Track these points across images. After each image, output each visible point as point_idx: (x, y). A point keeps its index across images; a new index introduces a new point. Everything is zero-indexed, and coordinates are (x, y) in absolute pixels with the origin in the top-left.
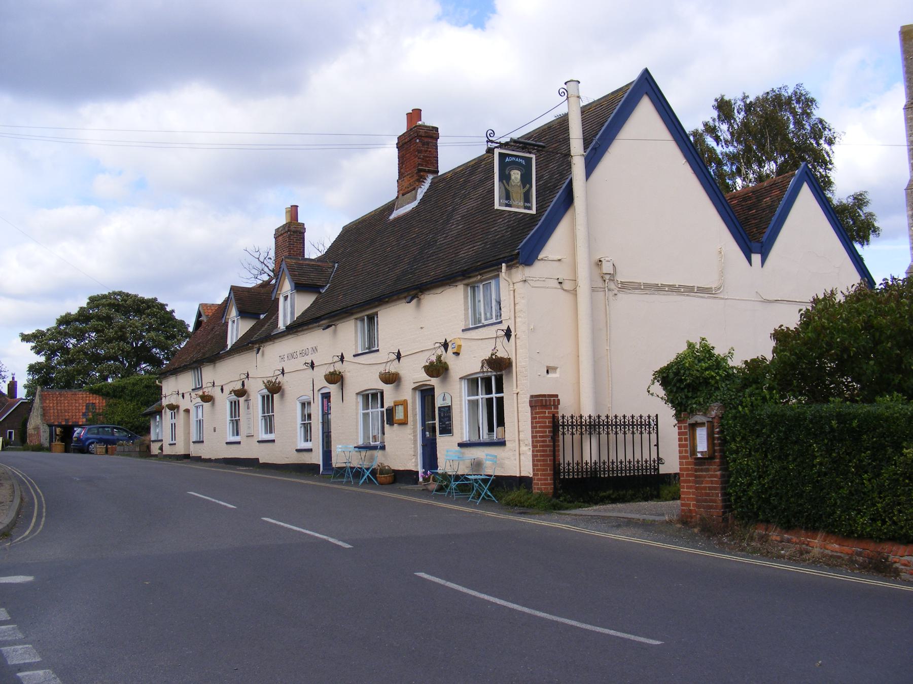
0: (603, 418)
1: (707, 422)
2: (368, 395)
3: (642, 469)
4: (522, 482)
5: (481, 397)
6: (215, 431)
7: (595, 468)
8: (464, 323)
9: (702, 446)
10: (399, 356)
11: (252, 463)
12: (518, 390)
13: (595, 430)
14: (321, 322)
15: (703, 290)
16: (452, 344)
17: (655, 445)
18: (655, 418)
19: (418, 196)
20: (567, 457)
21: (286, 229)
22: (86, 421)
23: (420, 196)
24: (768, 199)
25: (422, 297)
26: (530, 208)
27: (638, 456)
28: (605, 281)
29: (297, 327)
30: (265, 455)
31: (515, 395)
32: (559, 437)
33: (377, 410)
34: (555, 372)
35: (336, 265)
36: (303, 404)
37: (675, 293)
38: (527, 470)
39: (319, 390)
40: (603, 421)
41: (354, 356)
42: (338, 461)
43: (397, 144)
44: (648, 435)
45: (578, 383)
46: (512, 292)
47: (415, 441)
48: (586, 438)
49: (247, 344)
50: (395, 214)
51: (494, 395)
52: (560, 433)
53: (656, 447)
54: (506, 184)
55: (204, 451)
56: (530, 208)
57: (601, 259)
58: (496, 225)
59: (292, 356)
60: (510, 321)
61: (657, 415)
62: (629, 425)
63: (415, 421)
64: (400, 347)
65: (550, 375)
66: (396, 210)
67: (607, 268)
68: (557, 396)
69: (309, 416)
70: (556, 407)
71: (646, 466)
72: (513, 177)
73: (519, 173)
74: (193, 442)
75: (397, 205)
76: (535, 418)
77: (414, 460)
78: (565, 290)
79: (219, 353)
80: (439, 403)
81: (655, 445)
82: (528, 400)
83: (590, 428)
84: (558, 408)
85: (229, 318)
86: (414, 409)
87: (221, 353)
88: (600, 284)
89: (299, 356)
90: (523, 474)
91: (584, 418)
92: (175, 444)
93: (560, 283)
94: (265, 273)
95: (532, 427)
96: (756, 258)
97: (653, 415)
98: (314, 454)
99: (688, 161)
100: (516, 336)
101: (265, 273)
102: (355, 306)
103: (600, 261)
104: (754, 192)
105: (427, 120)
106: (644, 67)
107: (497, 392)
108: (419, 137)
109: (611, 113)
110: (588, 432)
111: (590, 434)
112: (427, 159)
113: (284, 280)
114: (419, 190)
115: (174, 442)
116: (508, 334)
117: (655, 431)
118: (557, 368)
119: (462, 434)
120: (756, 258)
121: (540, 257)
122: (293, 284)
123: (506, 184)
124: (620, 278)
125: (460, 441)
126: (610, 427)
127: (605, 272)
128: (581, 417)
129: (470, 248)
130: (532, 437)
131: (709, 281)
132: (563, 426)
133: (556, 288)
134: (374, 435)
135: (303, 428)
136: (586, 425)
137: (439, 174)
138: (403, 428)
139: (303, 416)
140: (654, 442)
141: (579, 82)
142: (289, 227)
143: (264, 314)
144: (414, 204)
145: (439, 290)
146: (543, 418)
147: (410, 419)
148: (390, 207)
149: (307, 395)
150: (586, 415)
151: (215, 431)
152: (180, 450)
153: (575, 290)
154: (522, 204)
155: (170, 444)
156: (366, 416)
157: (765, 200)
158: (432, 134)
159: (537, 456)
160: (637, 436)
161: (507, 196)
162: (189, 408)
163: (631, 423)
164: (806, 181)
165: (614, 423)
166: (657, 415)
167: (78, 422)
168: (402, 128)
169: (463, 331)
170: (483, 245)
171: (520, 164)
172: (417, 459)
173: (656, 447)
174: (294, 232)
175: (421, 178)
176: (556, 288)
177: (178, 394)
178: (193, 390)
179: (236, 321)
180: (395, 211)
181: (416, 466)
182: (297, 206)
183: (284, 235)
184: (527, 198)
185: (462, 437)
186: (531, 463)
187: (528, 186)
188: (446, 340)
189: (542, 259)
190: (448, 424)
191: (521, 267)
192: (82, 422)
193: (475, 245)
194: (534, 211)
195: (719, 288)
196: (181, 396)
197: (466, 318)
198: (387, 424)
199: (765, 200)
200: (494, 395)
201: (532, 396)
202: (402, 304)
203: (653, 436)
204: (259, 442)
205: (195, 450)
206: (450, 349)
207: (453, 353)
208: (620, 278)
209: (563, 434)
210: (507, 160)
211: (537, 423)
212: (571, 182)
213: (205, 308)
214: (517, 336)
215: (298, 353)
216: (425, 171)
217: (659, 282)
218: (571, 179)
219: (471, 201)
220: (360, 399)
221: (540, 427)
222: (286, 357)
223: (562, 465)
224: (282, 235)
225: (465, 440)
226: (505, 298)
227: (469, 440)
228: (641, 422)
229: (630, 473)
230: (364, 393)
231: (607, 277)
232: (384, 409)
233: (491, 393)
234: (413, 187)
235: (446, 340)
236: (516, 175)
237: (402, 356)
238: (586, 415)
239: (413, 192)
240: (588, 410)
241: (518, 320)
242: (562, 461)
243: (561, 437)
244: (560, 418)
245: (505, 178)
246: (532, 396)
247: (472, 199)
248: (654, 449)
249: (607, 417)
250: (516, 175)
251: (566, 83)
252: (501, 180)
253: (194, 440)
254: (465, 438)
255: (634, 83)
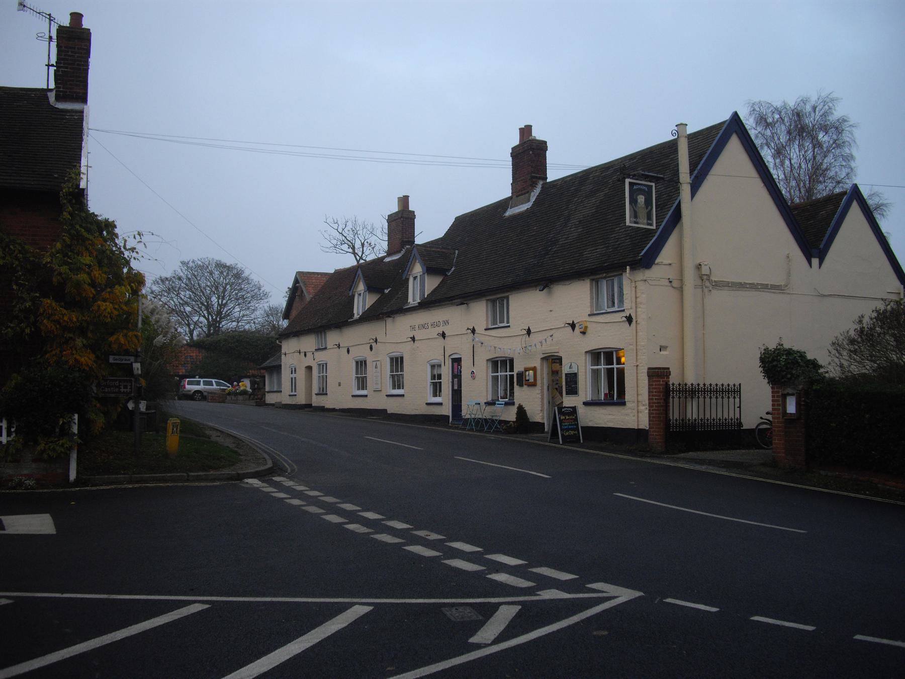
0: (701, 385)
1: (797, 393)
2: (498, 361)
3: (711, 426)
4: (639, 433)
5: (602, 367)
6: (340, 385)
7: (695, 424)
8: (590, 309)
9: (791, 408)
10: (529, 332)
11: (381, 414)
12: (638, 364)
13: (695, 395)
14: (454, 301)
15: (774, 287)
16: (580, 325)
17: (738, 407)
18: (738, 386)
19: (531, 198)
20: (675, 414)
21: (400, 216)
22: (186, 372)
23: (533, 199)
24: (824, 212)
25: (552, 286)
26: (651, 225)
27: (726, 416)
28: (703, 280)
29: (427, 304)
30: (393, 407)
31: (635, 367)
32: (669, 400)
33: (506, 373)
34: (666, 350)
35: (457, 252)
36: (433, 367)
37: (754, 290)
38: (644, 422)
39: (450, 356)
40: (702, 388)
41: (486, 330)
42: (465, 413)
43: (511, 154)
44: (709, 400)
45: (683, 358)
46: (634, 288)
47: (542, 399)
48: (689, 400)
49: (373, 315)
50: (509, 213)
51: (615, 366)
52: (671, 397)
53: (739, 409)
54: (634, 207)
55: (328, 402)
56: (651, 225)
57: (701, 263)
58: (615, 232)
59: (423, 327)
60: (631, 311)
61: (740, 384)
62: (720, 391)
63: (542, 383)
64: (530, 325)
65: (662, 353)
66: (511, 208)
67: (705, 270)
68: (669, 368)
69: (440, 377)
70: (668, 377)
71: (714, 424)
72: (639, 201)
73: (644, 197)
74: (316, 394)
75: (512, 204)
76: (652, 385)
77: (541, 414)
78: (673, 287)
79: (347, 321)
80: (566, 369)
81: (738, 407)
82: (646, 371)
83: (692, 394)
84: (669, 378)
85: (355, 292)
86: (542, 374)
87: (349, 321)
88: (699, 283)
89: (430, 327)
90: (640, 427)
91: (688, 386)
92: (296, 395)
93: (671, 282)
94: (345, 243)
95: (649, 392)
96: (815, 261)
97: (737, 384)
98: (444, 407)
99: (765, 185)
100: (636, 322)
101: (345, 243)
102: (489, 290)
103: (700, 265)
104: (812, 205)
105: (538, 134)
106: (735, 110)
107: (510, 372)
108: (532, 149)
109: (709, 147)
110: (690, 397)
111: (692, 398)
112: (539, 167)
113: (414, 263)
114: (532, 194)
115: (293, 393)
116: (629, 319)
117: (738, 397)
118: (667, 347)
119: (586, 395)
120: (815, 261)
121: (657, 262)
122: (425, 268)
123: (634, 207)
124: (713, 278)
125: (585, 401)
126: (688, 392)
127: (703, 273)
128: (686, 385)
129: (593, 250)
130: (649, 399)
131: (779, 281)
132: (673, 391)
133: (667, 286)
134: (605, 392)
135: (432, 386)
136: (689, 391)
137: (548, 180)
138: (531, 389)
139: (433, 377)
140: (737, 405)
141: (687, 125)
142: (402, 214)
143: (387, 289)
144: (529, 205)
145: (567, 283)
146: (659, 385)
147: (539, 382)
148: (503, 204)
149: (438, 358)
150: (689, 383)
151: (340, 385)
152: (301, 399)
153: (682, 288)
154: (645, 221)
155: (290, 395)
156: (495, 379)
157: (821, 213)
158: (540, 148)
159: (652, 414)
160: (714, 400)
161: (635, 215)
162: (312, 365)
163: (706, 392)
164: (856, 199)
165: (688, 392)
166: (740, 384)
167: (178, 373)
168: (516, 141)
169: (589, 315)
170: (605, 249)
171: (644, 190)
172: (543, 413)
173: (739, 409)
174: (406, 218)
175: (534, 183)
176: (667, 286)
177: (300, 352)
178: (316, 350)
179: (362, 294)
180: (509, 209)
181: (543, 418)
182: (409, 196)
183: (397, 221)
184: (649, 217)
185: (586, 398)
186: (648, 419)
187: (649, 207)
188: (573, 321)
189: (657, 264)
190: (574, 387)
191: (642, 270)
192: (182, 372)
193: (597, 247)
194: (654, 227)
195: (787, 286)
196: (303, 354)
197: (591, 306)
198: (517, 385)
199: (821, 213)
200: (615, 366)
201: (649, 369)
202: (533, 291)
203: (737, 400)
204: (387, 396)
205: (316, 401)
206: (577, 328)
207: (581, 332)
208: (713, 278)
209: (673, 397)
210: (635, 187)
211: (653, 388)
212: (679, 205)
213: (302, 275)
214: (638, 322)
215: (430, 325)
216: (536, 177)
217: (742, 281)
218: (680, 202)
219: (585, 208)
220: (490, 365)
221: (655, 392)
222: (417, 327)
223: (672, 421)
224: (395, 220)
225: (588, 400)
226: (627, 292)
227: (592, 400)
228: (722, 389)
229: (720, 428)
230: (494, 360)
231: (705, 277)
232: (515, 373)
233: (510, 375)
234: (527, 191)
235: (573, 321)
236: (641, 199)
237: (532, 332)
238: (540, 397)
239: (527, 195)
240: (691, 379)
241: (639, 310)
242: (671, 418)
243: (671, 399)
244: (671, 385)
245: (633, 201)
246: (649, 369)
247: (585, 207)
248: (737, 410)
249: (704, 385)
250: (641, 199)
251: (676, 126)
252: (630, 203)
253: (316, 393)
254: (589, 398)
255: (727, 123)
